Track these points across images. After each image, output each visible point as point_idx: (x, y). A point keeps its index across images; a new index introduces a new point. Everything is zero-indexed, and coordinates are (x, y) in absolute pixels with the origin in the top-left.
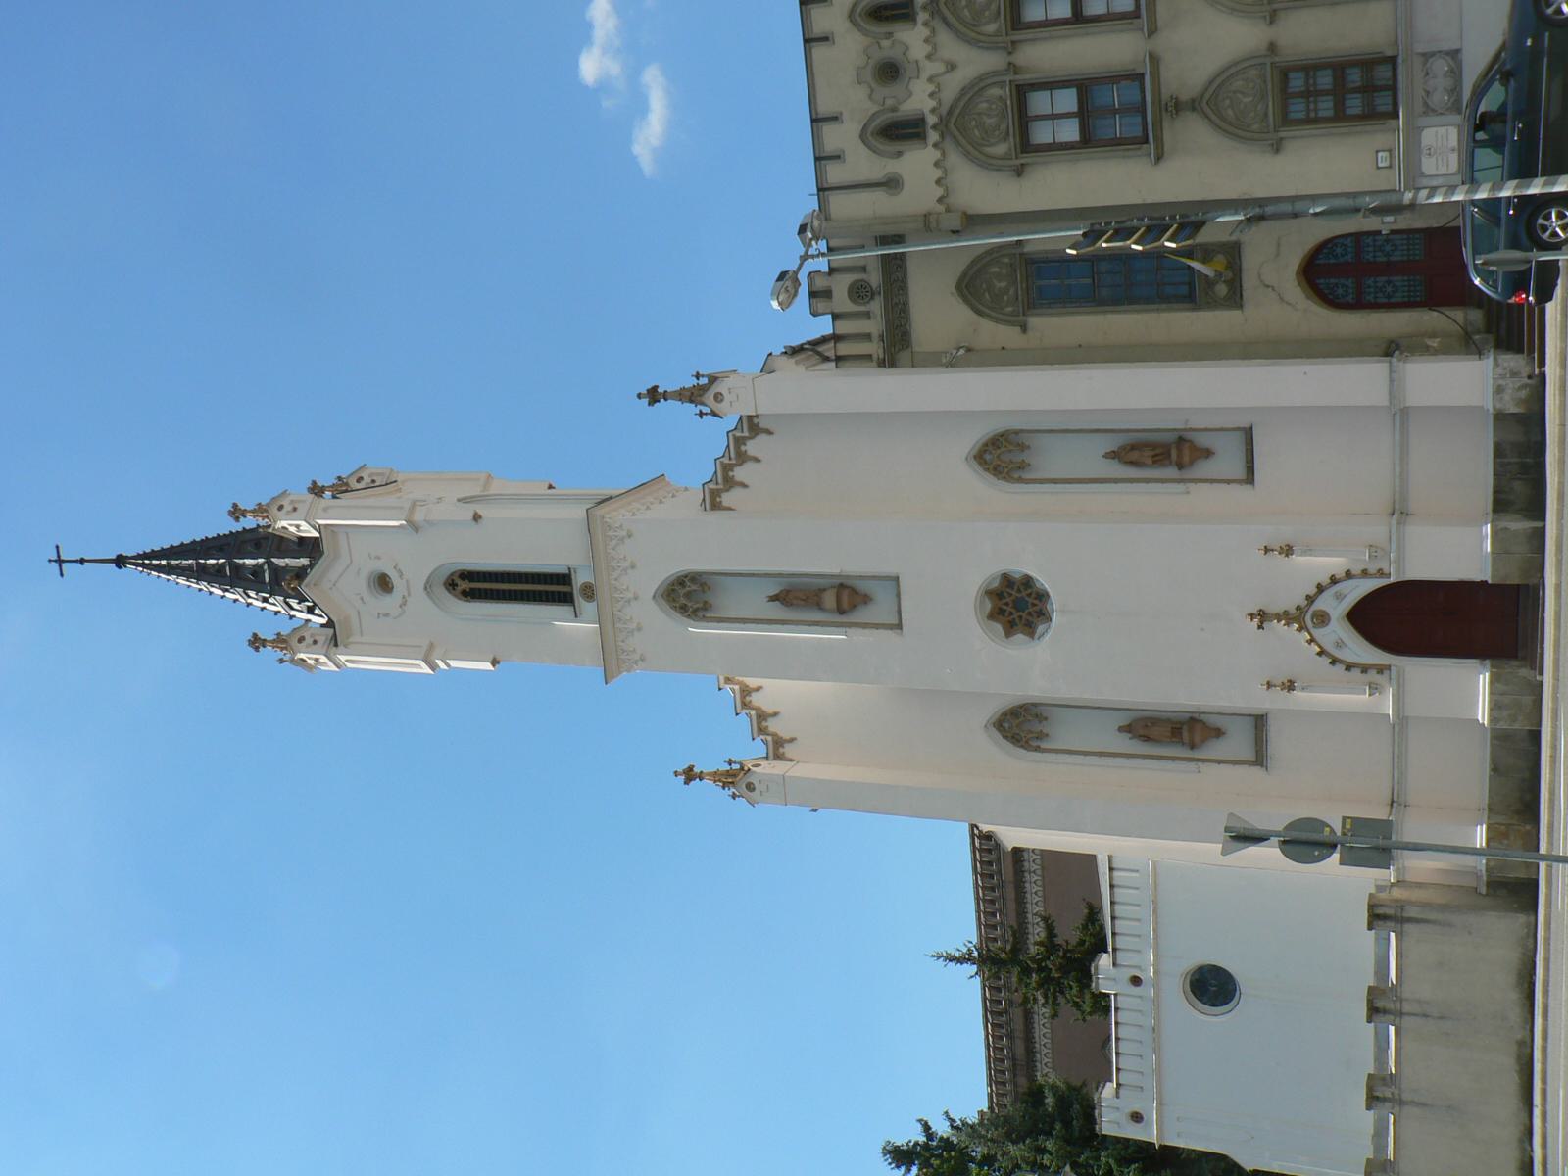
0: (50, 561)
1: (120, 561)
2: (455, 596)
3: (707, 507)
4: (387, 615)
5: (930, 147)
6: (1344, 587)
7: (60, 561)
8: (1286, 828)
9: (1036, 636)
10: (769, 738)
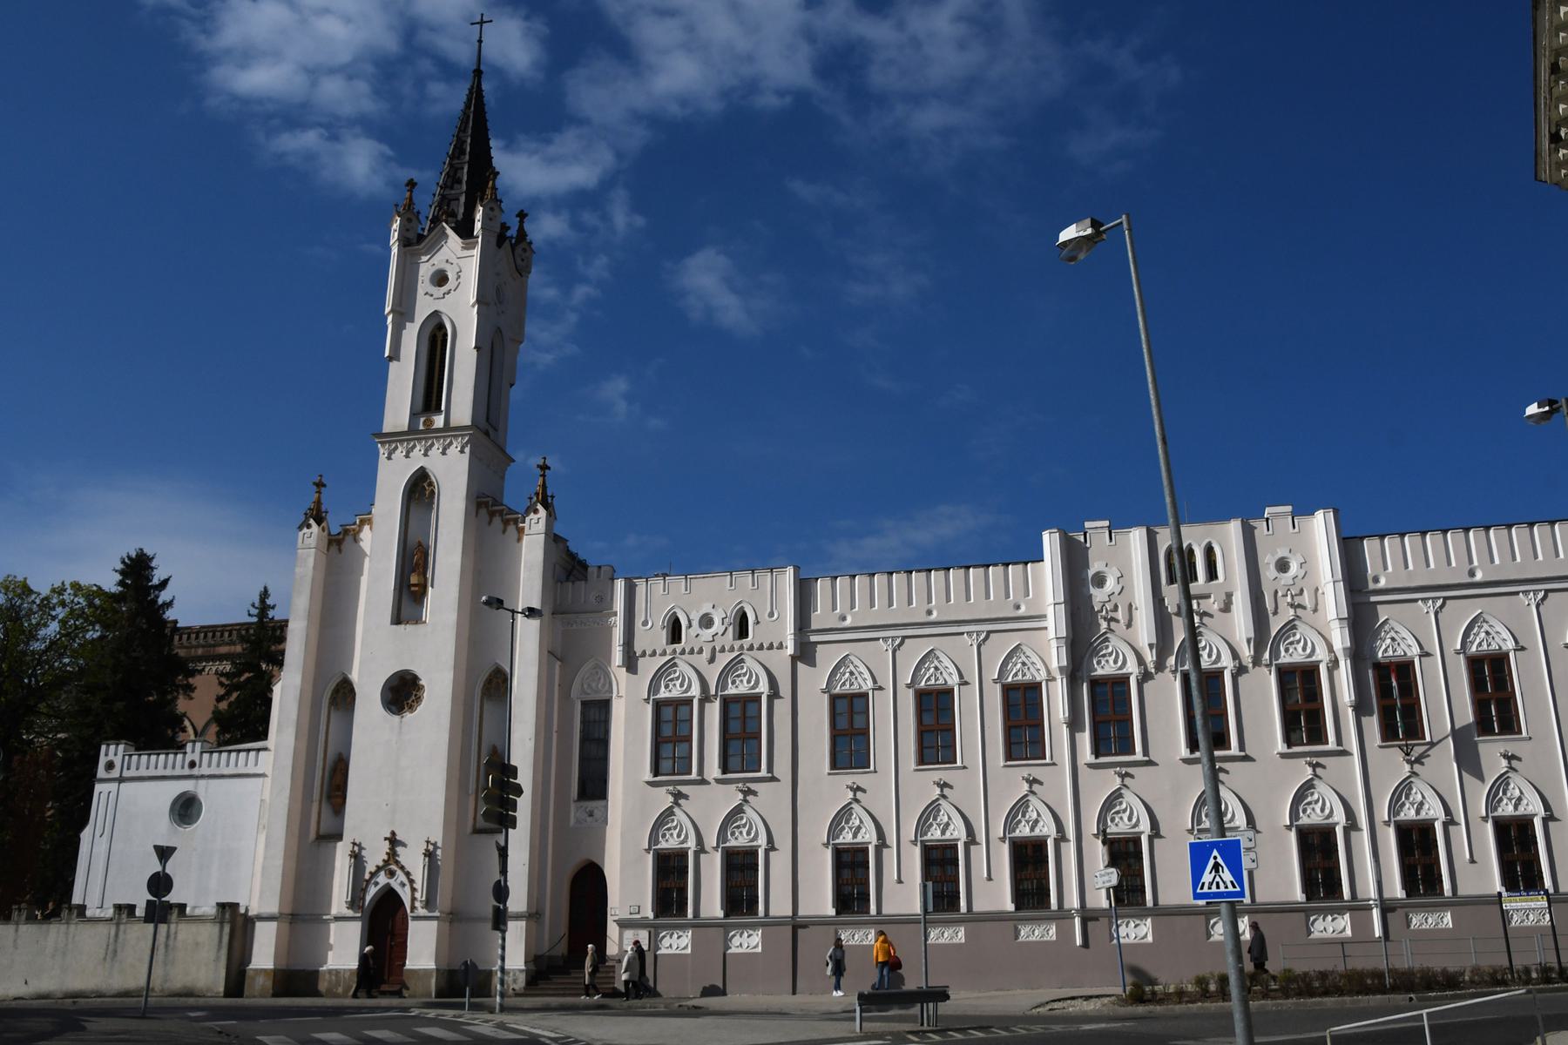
0: (482, 15)
2: (433, 331)
3: (479, 500)
4: (432, 295)
6: (408, 888)
7: (482, 23)
8: (167, 875)
9: (390, 706)
10: (341, 536)
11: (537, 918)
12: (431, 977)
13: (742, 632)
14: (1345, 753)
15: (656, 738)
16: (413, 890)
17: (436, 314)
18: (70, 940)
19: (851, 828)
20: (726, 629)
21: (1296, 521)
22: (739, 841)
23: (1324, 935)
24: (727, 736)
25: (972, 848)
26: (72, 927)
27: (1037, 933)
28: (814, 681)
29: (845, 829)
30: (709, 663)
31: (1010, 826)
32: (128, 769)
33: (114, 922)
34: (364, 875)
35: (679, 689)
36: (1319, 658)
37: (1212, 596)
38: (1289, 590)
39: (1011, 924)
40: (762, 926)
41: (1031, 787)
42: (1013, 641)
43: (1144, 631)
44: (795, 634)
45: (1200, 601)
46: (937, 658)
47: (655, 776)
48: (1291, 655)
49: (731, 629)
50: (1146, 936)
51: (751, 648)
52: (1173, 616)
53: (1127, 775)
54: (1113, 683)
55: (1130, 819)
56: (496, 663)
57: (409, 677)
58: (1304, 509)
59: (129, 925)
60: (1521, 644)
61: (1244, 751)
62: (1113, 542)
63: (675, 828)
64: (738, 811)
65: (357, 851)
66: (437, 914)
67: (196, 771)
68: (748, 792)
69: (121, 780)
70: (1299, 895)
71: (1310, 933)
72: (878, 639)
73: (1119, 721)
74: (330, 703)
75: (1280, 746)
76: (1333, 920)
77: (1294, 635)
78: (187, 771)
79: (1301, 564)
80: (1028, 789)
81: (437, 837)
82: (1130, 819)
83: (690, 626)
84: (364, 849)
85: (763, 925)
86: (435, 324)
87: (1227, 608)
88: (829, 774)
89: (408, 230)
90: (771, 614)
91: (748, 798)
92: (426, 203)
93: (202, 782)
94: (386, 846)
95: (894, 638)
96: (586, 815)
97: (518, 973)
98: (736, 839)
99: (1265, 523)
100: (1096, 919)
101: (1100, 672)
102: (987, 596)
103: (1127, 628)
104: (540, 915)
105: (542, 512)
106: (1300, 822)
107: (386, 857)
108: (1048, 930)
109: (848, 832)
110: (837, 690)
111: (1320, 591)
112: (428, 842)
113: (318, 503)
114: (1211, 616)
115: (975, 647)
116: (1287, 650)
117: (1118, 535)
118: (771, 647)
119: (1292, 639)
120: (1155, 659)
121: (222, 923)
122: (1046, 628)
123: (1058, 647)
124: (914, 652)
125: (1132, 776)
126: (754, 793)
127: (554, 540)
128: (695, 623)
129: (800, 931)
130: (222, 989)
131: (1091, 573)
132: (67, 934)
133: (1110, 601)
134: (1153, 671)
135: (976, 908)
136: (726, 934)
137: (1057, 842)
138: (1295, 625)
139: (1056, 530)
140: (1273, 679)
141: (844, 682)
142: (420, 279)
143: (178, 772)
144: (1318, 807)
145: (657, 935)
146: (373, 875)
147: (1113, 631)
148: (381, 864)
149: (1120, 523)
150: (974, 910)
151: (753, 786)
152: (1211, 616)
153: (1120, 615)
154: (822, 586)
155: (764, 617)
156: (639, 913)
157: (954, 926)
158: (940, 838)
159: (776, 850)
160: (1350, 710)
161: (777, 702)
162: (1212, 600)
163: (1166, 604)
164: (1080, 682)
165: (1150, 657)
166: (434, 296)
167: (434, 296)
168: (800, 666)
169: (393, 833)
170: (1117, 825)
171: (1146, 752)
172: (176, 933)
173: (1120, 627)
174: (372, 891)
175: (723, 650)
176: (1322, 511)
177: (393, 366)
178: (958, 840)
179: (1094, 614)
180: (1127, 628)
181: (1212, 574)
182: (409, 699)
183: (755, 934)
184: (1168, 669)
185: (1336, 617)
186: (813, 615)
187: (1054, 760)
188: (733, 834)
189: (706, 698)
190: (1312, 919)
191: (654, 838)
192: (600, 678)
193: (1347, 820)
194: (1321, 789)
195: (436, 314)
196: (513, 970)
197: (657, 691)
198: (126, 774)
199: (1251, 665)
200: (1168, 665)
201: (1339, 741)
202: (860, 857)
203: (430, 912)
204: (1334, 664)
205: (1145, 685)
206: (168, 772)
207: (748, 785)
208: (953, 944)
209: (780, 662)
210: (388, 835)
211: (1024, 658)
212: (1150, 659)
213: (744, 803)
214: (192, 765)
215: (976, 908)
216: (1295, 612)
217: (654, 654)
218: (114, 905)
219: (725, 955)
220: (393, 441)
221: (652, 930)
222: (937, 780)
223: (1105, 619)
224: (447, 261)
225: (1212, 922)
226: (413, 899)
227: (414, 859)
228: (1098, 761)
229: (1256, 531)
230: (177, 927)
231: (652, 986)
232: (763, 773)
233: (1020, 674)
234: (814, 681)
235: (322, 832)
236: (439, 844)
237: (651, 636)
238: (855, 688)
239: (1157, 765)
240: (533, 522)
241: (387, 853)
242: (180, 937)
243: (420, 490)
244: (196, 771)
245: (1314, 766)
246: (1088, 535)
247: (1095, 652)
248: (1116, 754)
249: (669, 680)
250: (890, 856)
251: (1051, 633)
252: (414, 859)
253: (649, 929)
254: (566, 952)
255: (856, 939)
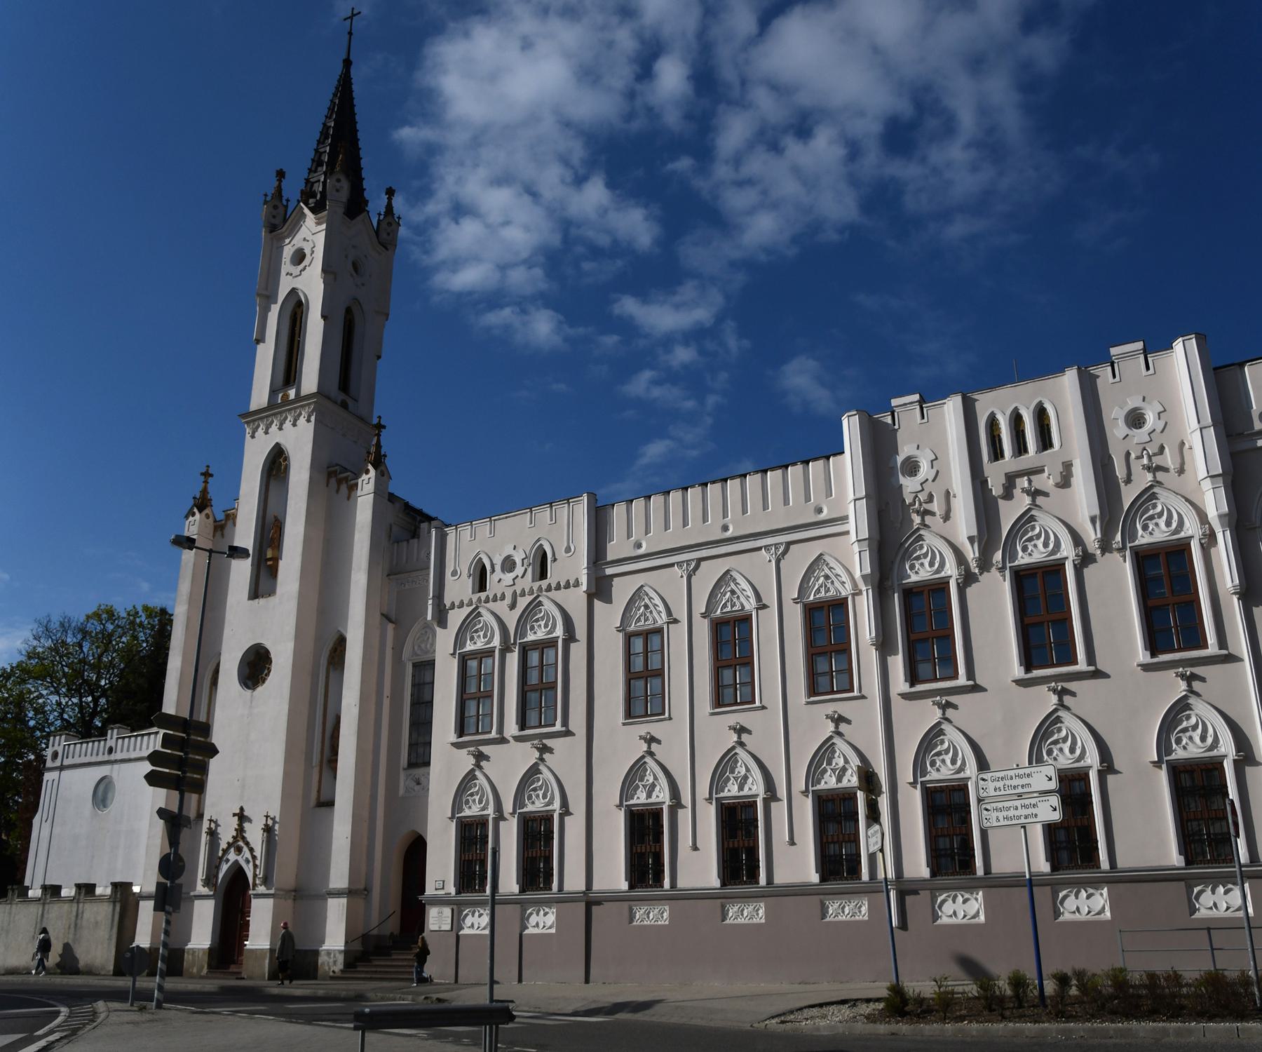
1: (347, 63)
4: (291, 274)
5: (527, 596)
6: (251, 864)
7: (351, 18)
11: (366, 895)
12: (265, 959)
13: (481, 585)
14: (1231, 658)
15: (523, 687)
16: (255, 866)
17: (294, 291)
18: (12, 919)
19: (833, 770)
20: (526, 570)
21: (1150, 360)
22: (535, 806)
23: (1214, 913)
24: (465, 696)
25: (773, 805)
26: (14, 906)
27: (655, 915)
28: (609, 616)
29: (827, 771)
30: (511, 610)
31: (813, 779)
32: (67, 758)
33: (42, 901)
34: (218, 852)
35: (929, 569)
36: (1190, 533)
37: (1046, 468)
38: (1145, 449)
39: (816, 899)
40: (1107, 883)
41: (837, 727)
42: (814, 550)
43: (964, 523)
44: (588, 568)
45: (1032, 477)
46: (734, 580)
47: (460, 736)
48: (1151, 533)
49: (530, 570)
50: (1102, 911)
51: (549, 589)
52: (999, 499)
53: (949, 705)
54: (1167, 553)
55: (1072, 750)
56: (339, 631)
57: (262, 651)
58: (1157, 343)
59: (51, 905)
60: (674, 617)
61: (1227, 648)
62: (1151, 371)
63: (947, 751)
64: (533, 771)
65: (271, 825)
66: (272, 892)
67: (113, 757)
68: (544, 749)
69: (62, 768)
70: (1175, 858)
71: (1193, 910)
72: (759, 549)
73: (1055, 622)
74: (211, 683)
75: (1142, 656)
76: (1226, 892)
77: (1155, 506)
78: (106, 758)
79: (1159, 414)
80: (645, 749)
81: (275, 812)
82: (1072, 750)
83: (493, 571)
84: (219, 826)
85: (1245, 876)
86: (295, 302)
87: (1065, 482)
88: (624, 724)
89: (274, 217)
90: (568, 550)
91: (544, 756)
92: (293, 188)
93: (116, 766)
94: (235, 822)
95: (688, 562)
96: (415, 784)
97: (337, 955)
98: (533, 803)
99: (1109, 369)
100: (915, 892)
101: (914, 578)
102: (786, 502)
103: (945, 522)
104: (368, 892)
105: (372, 472)
106: (1173, 757)
107: (234, 833)
108: (861, 907)
109: (831, 776)
110: (632, 628)
111: (1187, 446)
112: (267, 817)
113: (205, 491)
114: (1046, 495)
115: (774, 562)
116: (1145, 528)
117: (931, 411)
118: (567, 586)
119: (1151, 512)
120: (977, 555)
121: (114, 902)
122: (847, 533)
123: (860, 552)
124: (709, 574)
125: (955, 707)
126: (550, 750)
127: (385, 497)
128: (498, 568)
129: (595, 909)
130: (112, 968)
131: (900, 459)
132: (10, 913)
133: (923, 490)
134: (977, 571)
135: (996, 868)
136: (1055, 895)
137: (767, 802)
138: (920, 535)
139: (855, 412)
140: (1128, 568)
141: (725, 604)
142: (284, 260)
143: (100, 758)
144: (1196, 735)
145: (460, 912)
146: (225, 851)
147: (929, 527)
148: (231, 840)
149: (930, 395)
150: (775, 882)
151: (548, 742)
152: (1046, 495)
153: (936, 506)
154: (618, 512)
155: (561, 553)
156: (443, 888)
157: (738, 903)
158: (737, 794)
159: (571, 814)
160: (1235, 598)
161: (573, 646)
162: (1046, 474)
163: (990, 487)
164: (890, 592)
165: (971, 553)
166: (293, 275)
167: (293, 275)
168: (597, 603)
169: (242, 809)
170: (1185, 748)
171: (971, 674)
172: (83, 913)
173: (935, 522)
174: (225, 867)
175: (523, 594)
176: (1180, 339)
177: (260, 347)
178: (757, 796)
179: (905, 508)
180: (945, 522)
181: (1045, 441)
182: (262, 674)
183: (1097, 894)
184: (994, 567)
185: (1206, 475)
186: (609, 546)
187: (863, 693)
188: (933, 764)
189: (506, 649)
190: (1196, 890)
191: (1164, 745)
192: (428, 638)
193: (1238, 750)
194: (1201, 710)
195: (294, 291)
196: (334, 950)
197: (463, 645)
198: (66, 762)
199: (1098, 552)
200: (994, 562)
201: (1222, 642)
202: (957, 798)
203: (268, 889)
204: (1209, 539)
205: (969, 590)
206: (94, 759)
207: (544, 741)
208: (753, 924)
209: (576, 601)
210: (238, 811)
211: (827, 571)
212: (972, 556)
213: (539, 762)
214: (111, 751)
215: (996, 868)
216: (1155, 477)
217: (461, 605)
218: (112, 883)
219: (521, 936)
220: (295, 408)
221: (455, 907)
222: (732, 723)
223: (918, 512)
224: (305, 239)
225: (1061, 895)
226: (255, 876)
227: (255, 835)
228: (913, 690)
229: (1098, 381)
230: (83, 907)
231: (231, 970)
232: (962, 680)
233: (823, 590)
234: (609, 616)
235: (322, 799)
236: (277, 819)
237: (459, 588)
238: (649, 625)
239: (985, 690)
240: (364, 482)
241: (236, 830)
242: (85, 916)
243: (277, 464)
244: (113, 757)
245: (1190, 679)
246: (896, 414)
247: (907, 555)
248: (1180, 650)
249: (1026, 541)
250: (684, 816)
251: (853, 537)
252: (255, 835)
253: (451, 906)
254: (397, 932)
255: (847, 912)
